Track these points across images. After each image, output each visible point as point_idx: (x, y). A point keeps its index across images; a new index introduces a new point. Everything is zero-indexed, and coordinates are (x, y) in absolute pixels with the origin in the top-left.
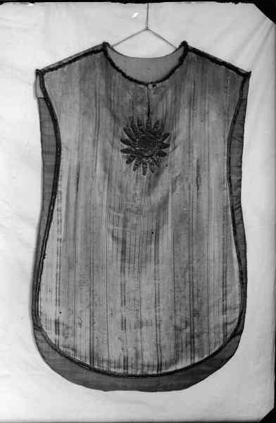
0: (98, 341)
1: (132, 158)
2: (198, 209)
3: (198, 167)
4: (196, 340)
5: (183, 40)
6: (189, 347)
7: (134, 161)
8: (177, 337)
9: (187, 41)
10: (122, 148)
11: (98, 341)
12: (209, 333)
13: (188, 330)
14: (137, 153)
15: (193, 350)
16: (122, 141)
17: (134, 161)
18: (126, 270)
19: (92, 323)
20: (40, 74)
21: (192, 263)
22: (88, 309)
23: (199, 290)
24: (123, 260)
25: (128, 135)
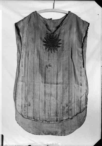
0: (36, 111)
1: (47, 47)
2: (71, 72)
3: (72, 48)
4: (70, 111)
5: (35, 10)
6: (67, 114)
7: (48, 48)
8: (63, 110)
9: (90, 23)
10: (44, 44)
11: (36, 111)
12: (74, 109)
13: (67, 108)
14: (49, 45)
15: (69, 115)
16: (43, 41)
17: (48, 48)
18: (46, 86)
19: (34, 105)
20: (16, 25)
21: (70, 84)
22: (32, 100)
23: (71, 94)
24: (45, 83)
25: (46, 40)
